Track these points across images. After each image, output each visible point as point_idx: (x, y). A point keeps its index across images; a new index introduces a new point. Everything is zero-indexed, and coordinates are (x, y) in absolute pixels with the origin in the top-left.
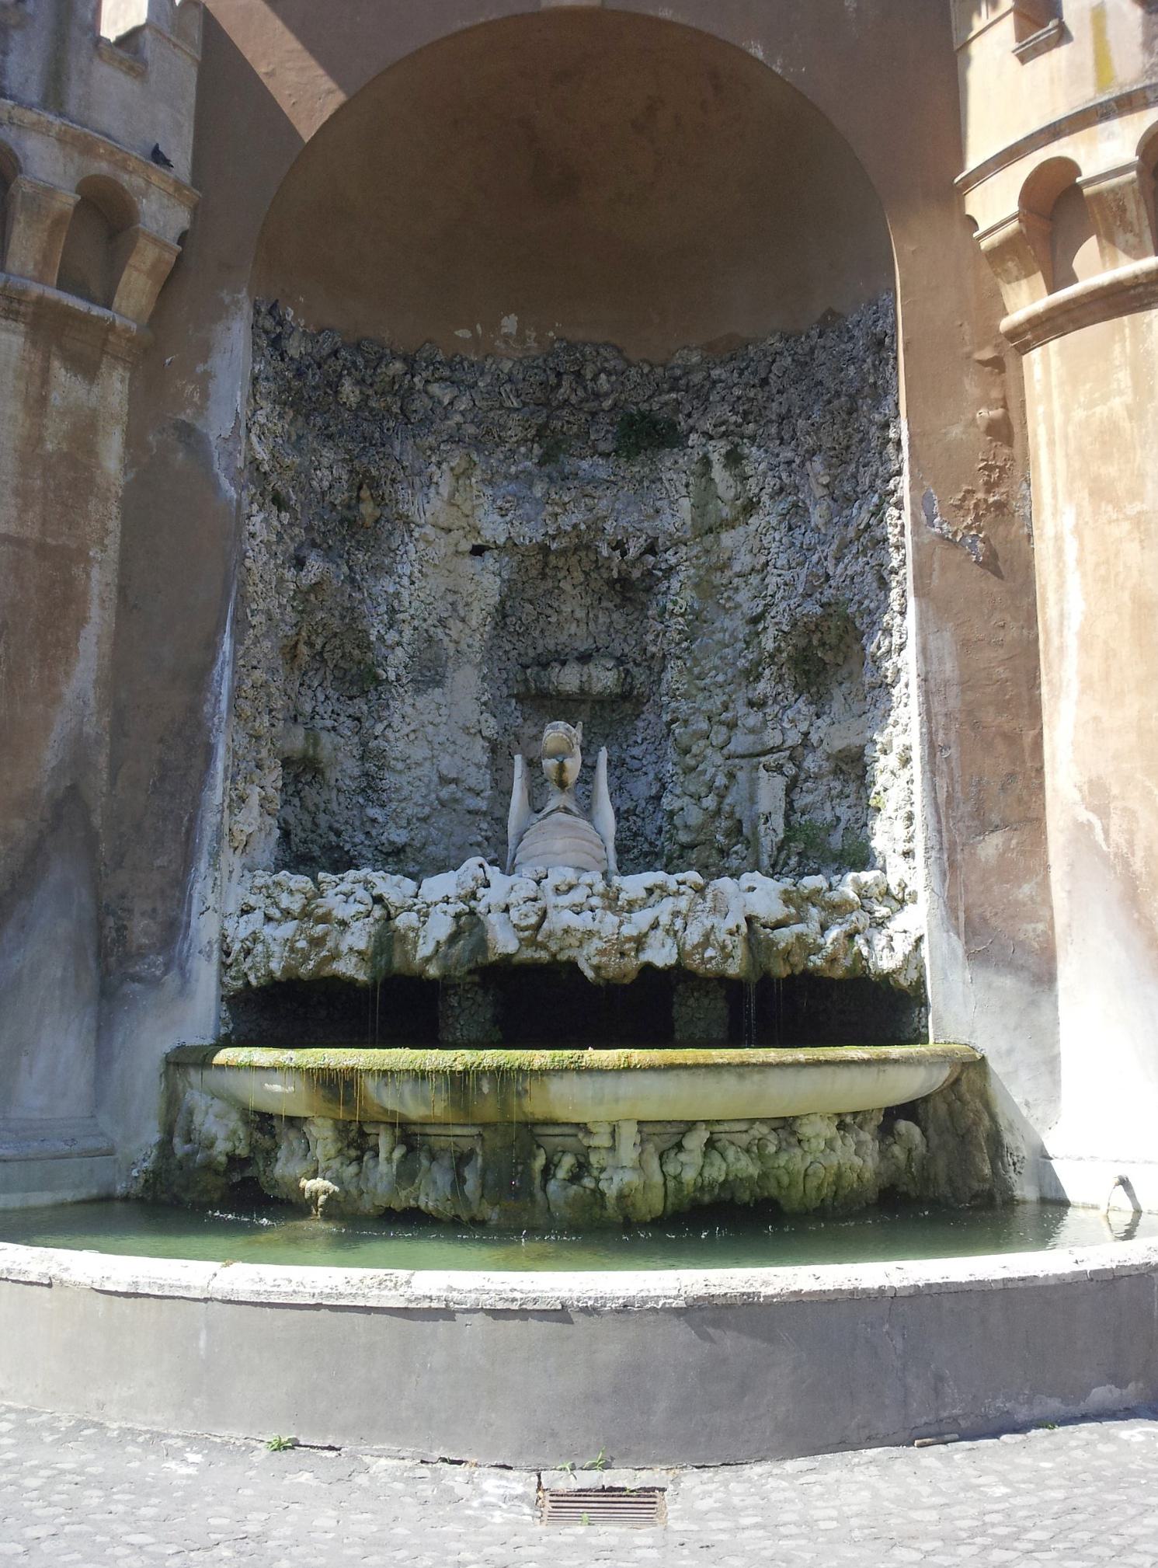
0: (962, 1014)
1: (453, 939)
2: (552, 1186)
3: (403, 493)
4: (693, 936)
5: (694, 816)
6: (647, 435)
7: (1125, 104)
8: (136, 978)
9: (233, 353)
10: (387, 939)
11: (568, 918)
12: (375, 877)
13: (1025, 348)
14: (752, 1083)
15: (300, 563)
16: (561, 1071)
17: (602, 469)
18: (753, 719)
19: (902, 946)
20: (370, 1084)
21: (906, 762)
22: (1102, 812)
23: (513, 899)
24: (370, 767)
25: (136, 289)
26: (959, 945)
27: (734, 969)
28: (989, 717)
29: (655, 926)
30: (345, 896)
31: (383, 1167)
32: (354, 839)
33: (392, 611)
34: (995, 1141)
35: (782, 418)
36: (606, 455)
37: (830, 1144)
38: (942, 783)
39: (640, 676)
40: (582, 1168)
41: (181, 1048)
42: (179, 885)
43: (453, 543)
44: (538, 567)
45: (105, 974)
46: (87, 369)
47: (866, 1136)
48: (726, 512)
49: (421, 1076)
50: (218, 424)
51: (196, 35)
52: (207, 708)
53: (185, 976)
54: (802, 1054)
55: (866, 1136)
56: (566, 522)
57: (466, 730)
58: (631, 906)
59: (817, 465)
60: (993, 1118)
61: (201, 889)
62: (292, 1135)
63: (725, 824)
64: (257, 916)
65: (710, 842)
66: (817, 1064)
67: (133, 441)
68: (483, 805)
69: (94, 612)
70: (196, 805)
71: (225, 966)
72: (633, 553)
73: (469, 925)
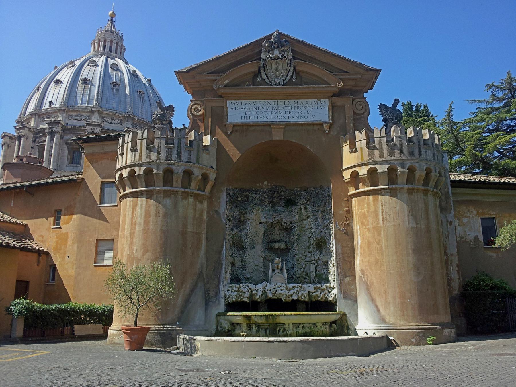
0: (342, 307)
1: (262, 295)
2: (280, 333)
3: (248, 215)
4: (300, 295)
5: (300, 272)
6: (290, 203)
7: (365, 164)
8: (211, 302)
9: (224, 197)
10: (252, 295)
11: (280, 292)
13: (352, 198)
15: (232, 230)
17: (283, 209)
18: (310, 255)
19: (333, 296)
20: (253, 317)
21: (334, 266)
22: (363, 275)
24: (243, 263)
25: (208, 188)
26: (342, 296)
27: (306, 300)
28: (346, 259)
29: (294, 293)
30: (245, 287)
31: (254, 330)
32: (240, 276)
33: (246, 236)
34: (348, 327)
35: (314, 202)
36: (283, 207)
37: (321, 327)
39: (289, 245)
40: (284, 330)
41: (219, 313)
42: (218, 286)
45: (206, 301)
46: (201, 202)
48: (304, 218)
49: (261, 316)
50: (222, 210)
51: (216, 143)
53: (219, 301)
54: (316, 313)
55: (327, 326)
56: (276, 219)
57: (259, 256)
58: (290, 290)
59: (319, 212)
60: (347, 323)
61: (221, 287)
64: (230, 291)
65: (302, 277)
66: (319, 314)
67: (208, 213)
68: (262, 269)
69: (203, 242)
70: (220, 273)
71: (225, 300)
72: (288, 224)
73: (264, 293)
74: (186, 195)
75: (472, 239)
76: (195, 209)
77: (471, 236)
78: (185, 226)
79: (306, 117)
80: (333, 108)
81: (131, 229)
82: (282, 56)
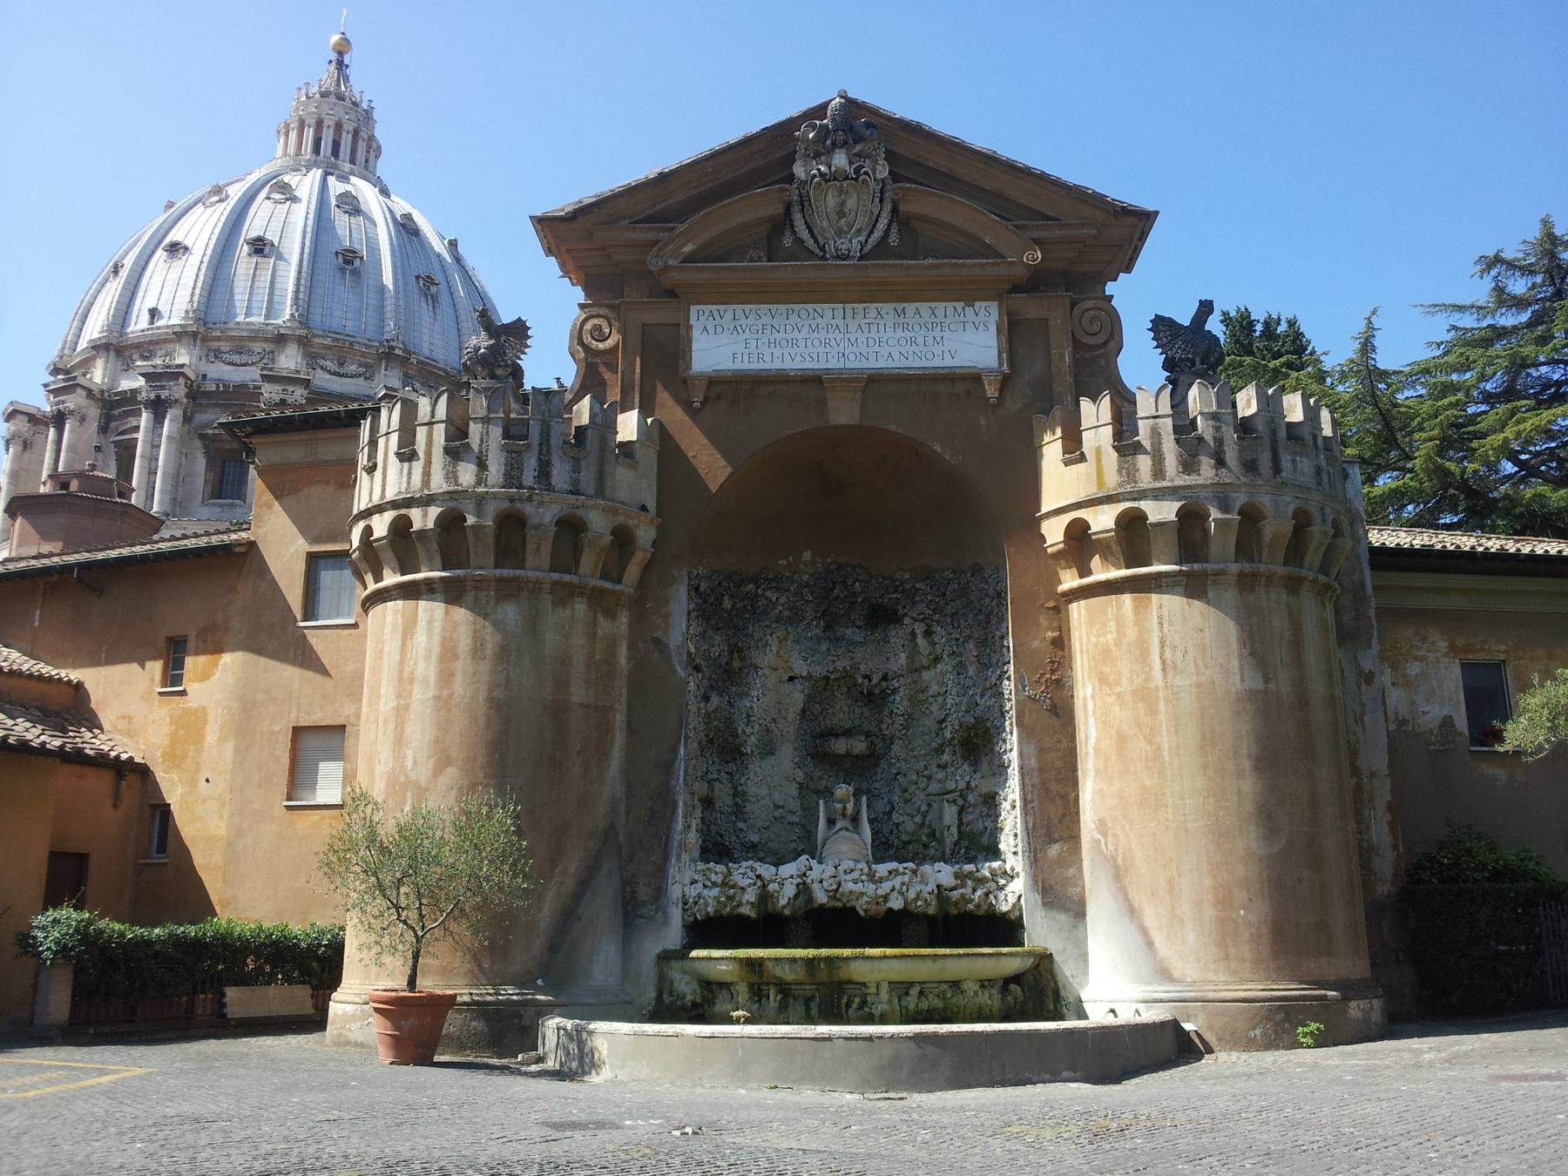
0: (1040, 932)
1: (796, 896)
4: (912, 895)
6: (881, 617)
7: (1110, 499)
8: (642, 917)
9: (680, 601)
10: (765, 896)
11: (851, 886)
12: (757, 865)
13: (1071, 602)
14: (939, 964)
15: (706, 698)
16: (857, 958)
17: (859, 636)
18: (941, 775)
19: (1012, 899)
20: (770, 965)
22: (1105, 835)
23: (824, 876)
25: (633, 571)
26: (1039, 898)
27: (931, 911)
28: (1054, 787)
29: (893, 890)
31: (772, 1004)
32: (730, 840)
33: (749, 716)
35: (953, 615)
36: (859, 627)
37: (975, 993)
38: (1030, 819)
40: (864, 1003)
41: (665, 951)
42: (662, 870)
43: (780, 676)
44: (821, 689)
46: (611, 615)
47: (994, 991)
48: (925, 662)
49: (794, 960)
52: (673, 783)
53: (666, 915)
54: (961, 951)
55: (994, 991)
56: (839, 665)
57: (787, 778)
58: (881, 880)
59: (971, 645)
60: (1056, 983)
61: (673, 872)
62: (724, 991)
63: (926, 831)
64: (700, 885)
66: (968, 955)
67: (632, 647)
70: (669, 830)
72: (875, 681)
74: (564, 595)
75: (1434, 725)
76: (592, 636)
77: (1432, 714)
78: (562, 686)
79: (930, 356)
80: (1013, 331)
81: (399, 696)
82: (857, 171)
